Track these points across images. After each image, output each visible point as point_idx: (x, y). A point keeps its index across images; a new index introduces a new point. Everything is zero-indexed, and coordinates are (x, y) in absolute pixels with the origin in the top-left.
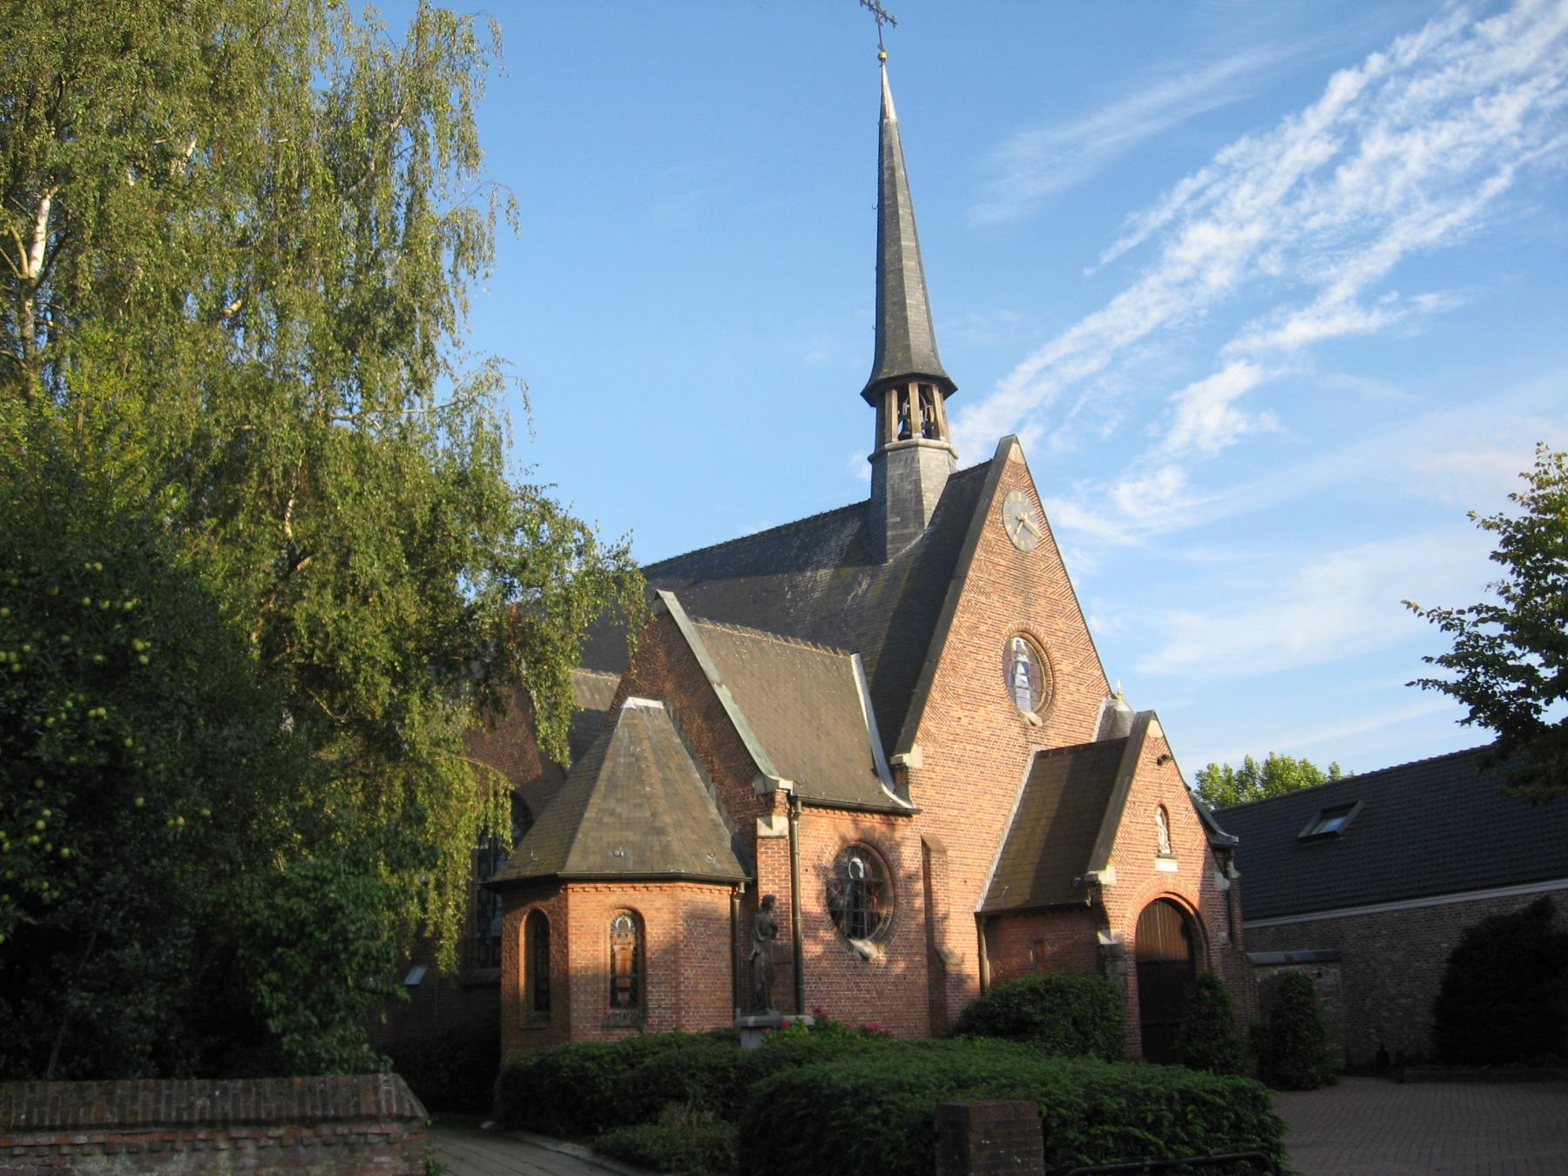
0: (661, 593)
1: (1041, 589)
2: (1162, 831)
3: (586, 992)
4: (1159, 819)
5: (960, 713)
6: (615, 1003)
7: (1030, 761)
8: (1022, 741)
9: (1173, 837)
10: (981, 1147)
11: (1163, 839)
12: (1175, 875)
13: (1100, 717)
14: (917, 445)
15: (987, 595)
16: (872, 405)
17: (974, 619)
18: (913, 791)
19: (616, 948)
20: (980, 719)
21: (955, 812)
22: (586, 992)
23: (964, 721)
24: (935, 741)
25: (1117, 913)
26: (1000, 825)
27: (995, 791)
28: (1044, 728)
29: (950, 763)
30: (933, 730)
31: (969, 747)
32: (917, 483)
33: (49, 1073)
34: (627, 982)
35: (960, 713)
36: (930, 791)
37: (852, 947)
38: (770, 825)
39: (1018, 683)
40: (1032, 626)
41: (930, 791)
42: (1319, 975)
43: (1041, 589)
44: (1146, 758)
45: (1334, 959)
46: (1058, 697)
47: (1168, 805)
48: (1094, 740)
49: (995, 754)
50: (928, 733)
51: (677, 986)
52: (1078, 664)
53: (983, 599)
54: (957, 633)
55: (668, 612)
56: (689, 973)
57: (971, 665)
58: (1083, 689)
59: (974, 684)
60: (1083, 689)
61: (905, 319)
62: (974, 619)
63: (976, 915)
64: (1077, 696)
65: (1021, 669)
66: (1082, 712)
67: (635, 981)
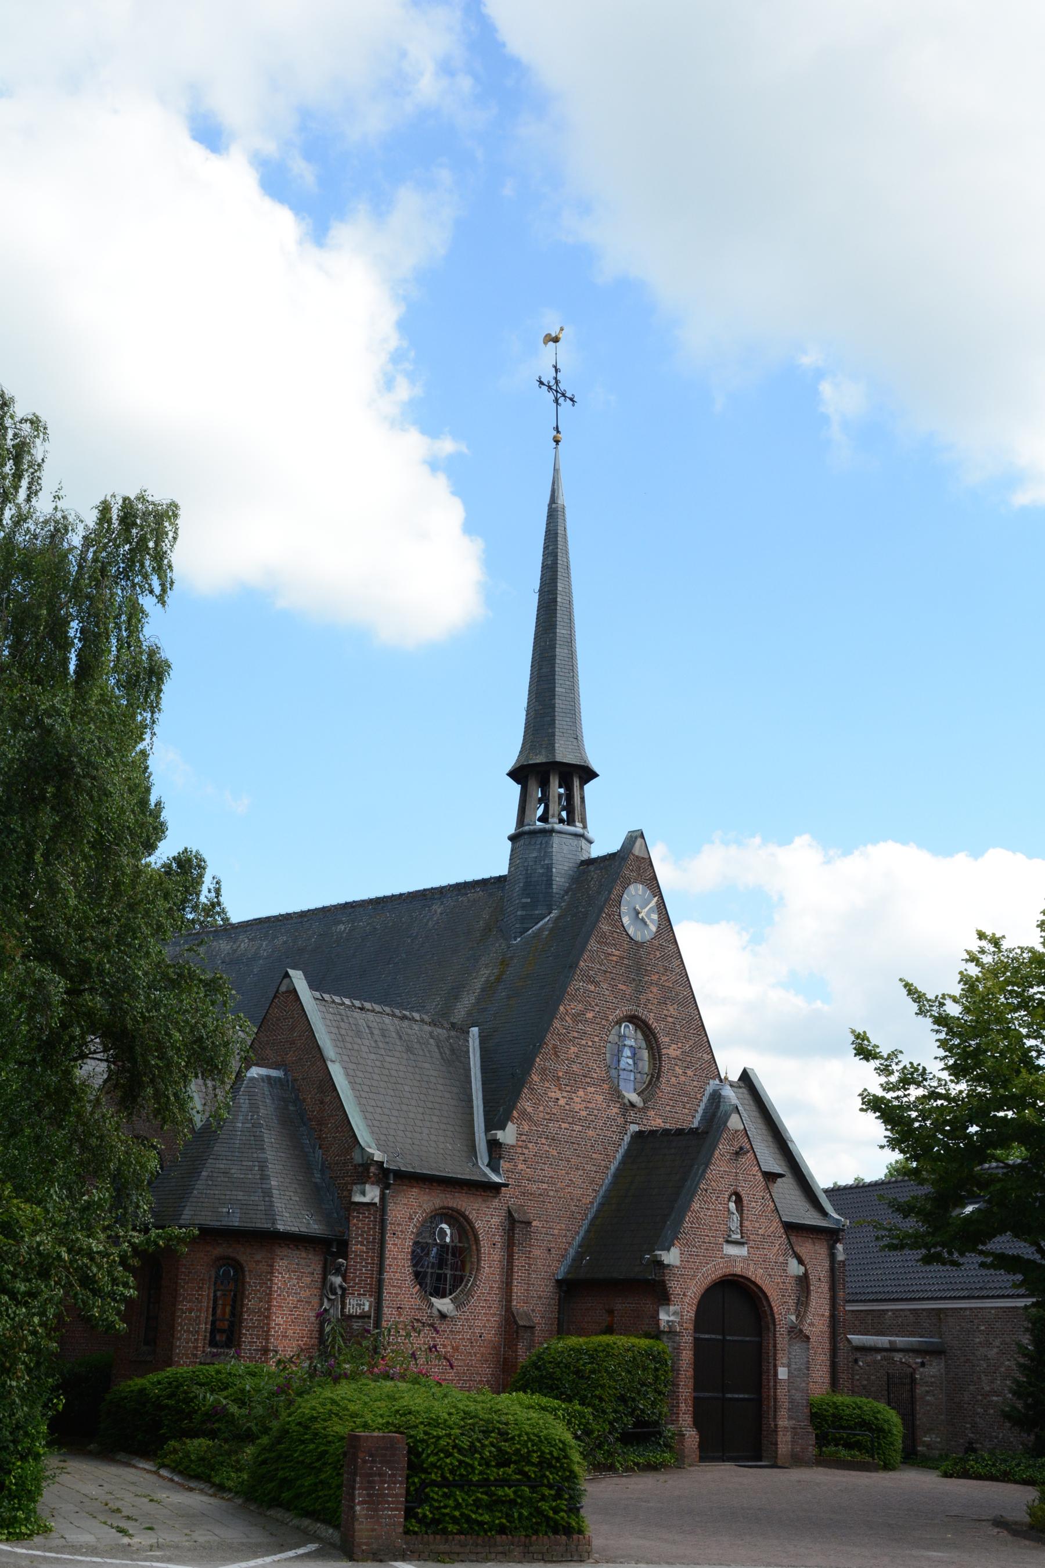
0: (291, 972)
1: (655, 977)
2: (736, 1217)
3: (188, 1331)
4: (732, 1206)
5: (559, 1095)
6: (213, 1343)
7: (627, 1139)
8: (620, 1120)
9: (746, 1223)
10: (365, 1462)
11: (735, 1224)
12: (745, 1259)
13: (705, 1099)
14: (552, 831)
15: (597, 984)
16: (518, 783)
17: (580, 1007)
18: (504, 1165)
19: (219, 1293)
20: (578, 1100)
21: (545, 1186)
22: (188, 1331)
23: (562, 1102)
24: (530, 1119)
25: (678, 1291)
26: (589, 1199)
27: (588, 1167)
28: (645, 1109)
29: (544, 1141)
30: (530, 1110)
31: (564, 1125)
32: (549, 868)
33: (696, 1394)
34: (226, 1325)
35: (559, 1095)
36: (521, 1166)
37: (431, 1305)
38: (363, 1193)
39: (622, 1065)
40: (642, 1013)
41: (521, 1166)
42: (923, 1364)
43: (655, 977)
44: (723, 1148)
45: (936, 1352)
46: (663, 1080)
47: (743, 1193)
48: (695, 1125)
49: (590, 1133)
50: (524, 1113)
51: (268, 1331)
52: (687, 1048)
53: (592, 988)
54: (562, 1019)
55: (295, 989)
56: (280, 1320)
57: (574, 1049)
58: (689, 1072)
59: (575, 1068)
60: (689, 1072)
61: (553, 707)
62: (580, 1007)
63: (558, 1281)
64: (683, 1078)
65: (627, 1052)
66: (687, 1095)
67: (232, 1324)
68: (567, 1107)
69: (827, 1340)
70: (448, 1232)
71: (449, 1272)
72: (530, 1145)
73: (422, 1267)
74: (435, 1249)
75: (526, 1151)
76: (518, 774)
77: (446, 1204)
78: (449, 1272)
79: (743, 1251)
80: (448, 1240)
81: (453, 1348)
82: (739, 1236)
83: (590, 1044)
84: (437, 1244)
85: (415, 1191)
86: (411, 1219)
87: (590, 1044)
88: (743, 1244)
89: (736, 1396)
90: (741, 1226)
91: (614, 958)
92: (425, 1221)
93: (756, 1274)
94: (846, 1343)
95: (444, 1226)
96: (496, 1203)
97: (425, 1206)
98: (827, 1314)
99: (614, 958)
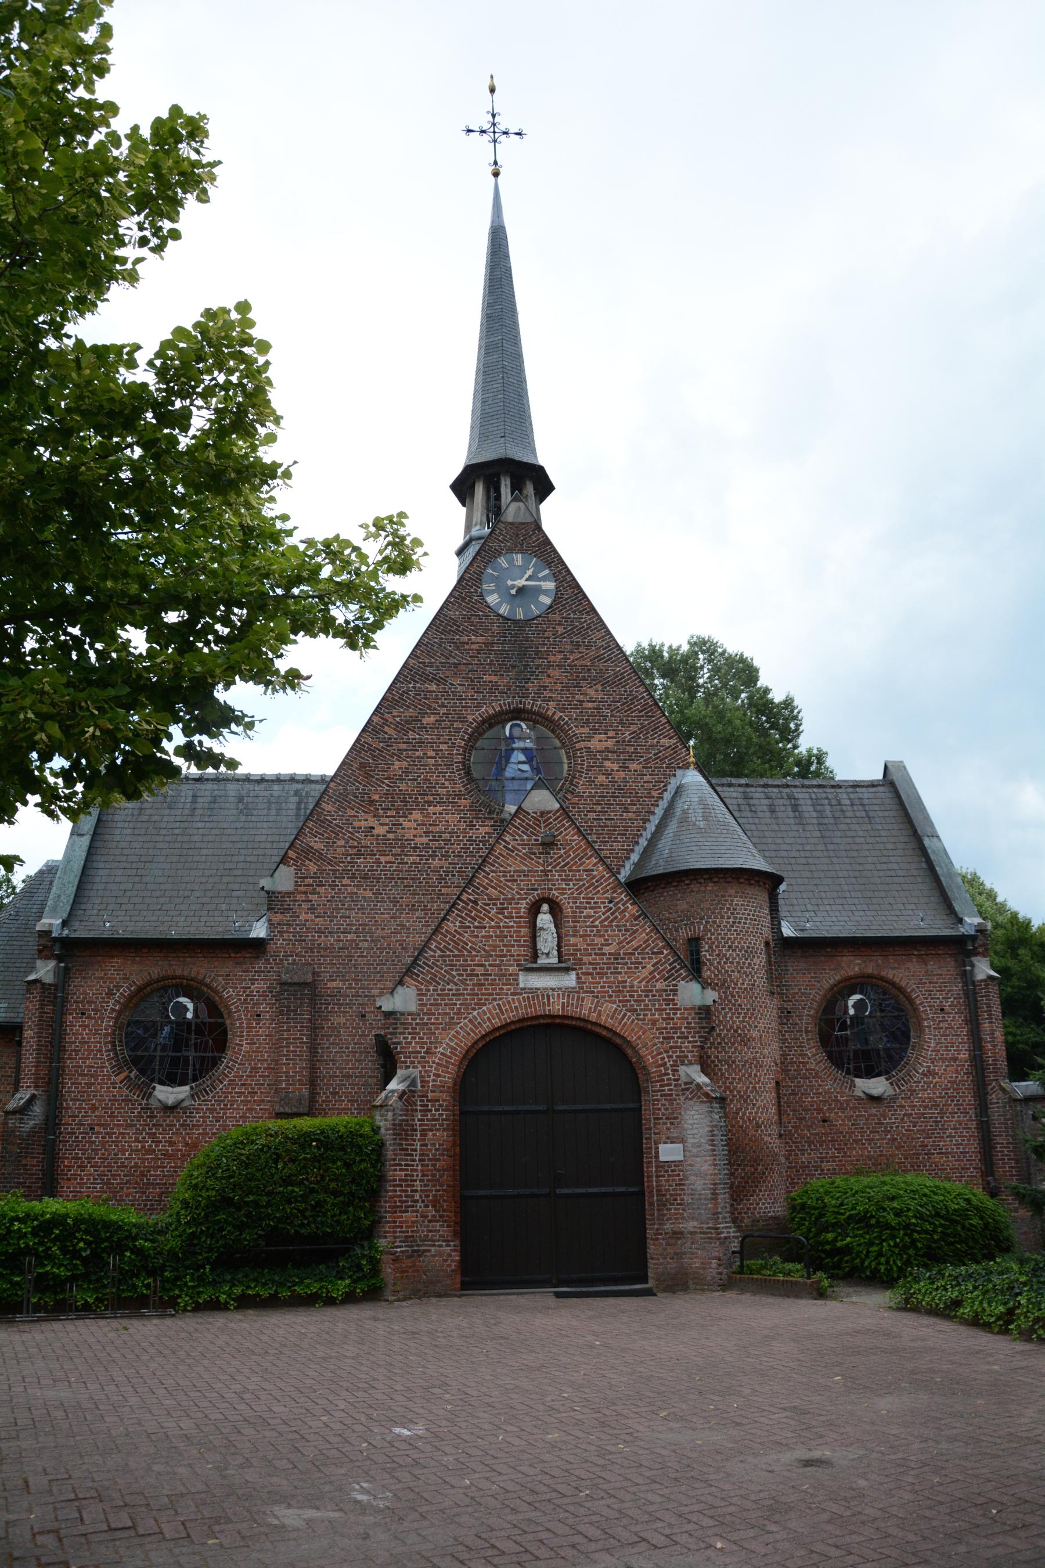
29: (346, 881)
31: (383, 859)
68: (391, 836)
69: (969, 1098)
70: (190, 1006)
71: (191, 1054)
72: (322, 890)
73: (146, 1049)
74: (167, 1029)
75: (315, 897)
76: (462, 488)
77: (170, 973)
78: (191, 1054)
79: (570, 980)
80: (189, 1015)
81: (187, 1144)
82: (555, 960)
83: (431, 753)
84: (171, 1022)
85: (117, 961)
86: (110, 994)
87: (431, 753)
88: (567, 970)
89: (590, 1190)
90: (559, 946)
91: (474, 646)
92: (131, 997)
93: (604, 1012)
94: (1001, 1095)
95: (182, 999)
96: (260, 965)
97: (134, 978)
98: (964, 1055)
99: (474, 646)
